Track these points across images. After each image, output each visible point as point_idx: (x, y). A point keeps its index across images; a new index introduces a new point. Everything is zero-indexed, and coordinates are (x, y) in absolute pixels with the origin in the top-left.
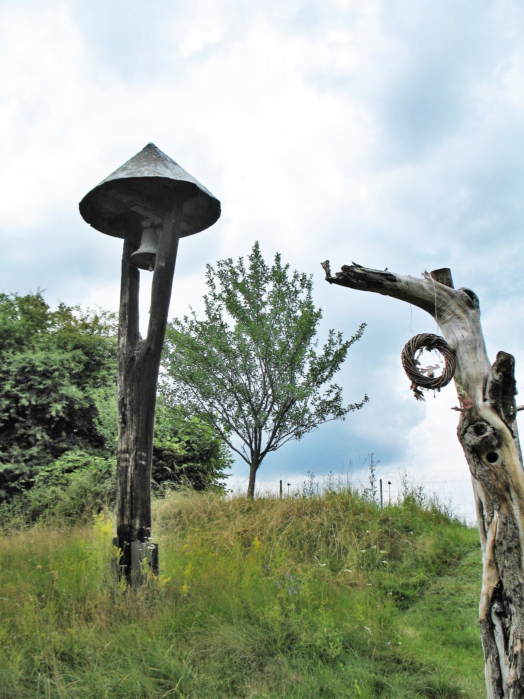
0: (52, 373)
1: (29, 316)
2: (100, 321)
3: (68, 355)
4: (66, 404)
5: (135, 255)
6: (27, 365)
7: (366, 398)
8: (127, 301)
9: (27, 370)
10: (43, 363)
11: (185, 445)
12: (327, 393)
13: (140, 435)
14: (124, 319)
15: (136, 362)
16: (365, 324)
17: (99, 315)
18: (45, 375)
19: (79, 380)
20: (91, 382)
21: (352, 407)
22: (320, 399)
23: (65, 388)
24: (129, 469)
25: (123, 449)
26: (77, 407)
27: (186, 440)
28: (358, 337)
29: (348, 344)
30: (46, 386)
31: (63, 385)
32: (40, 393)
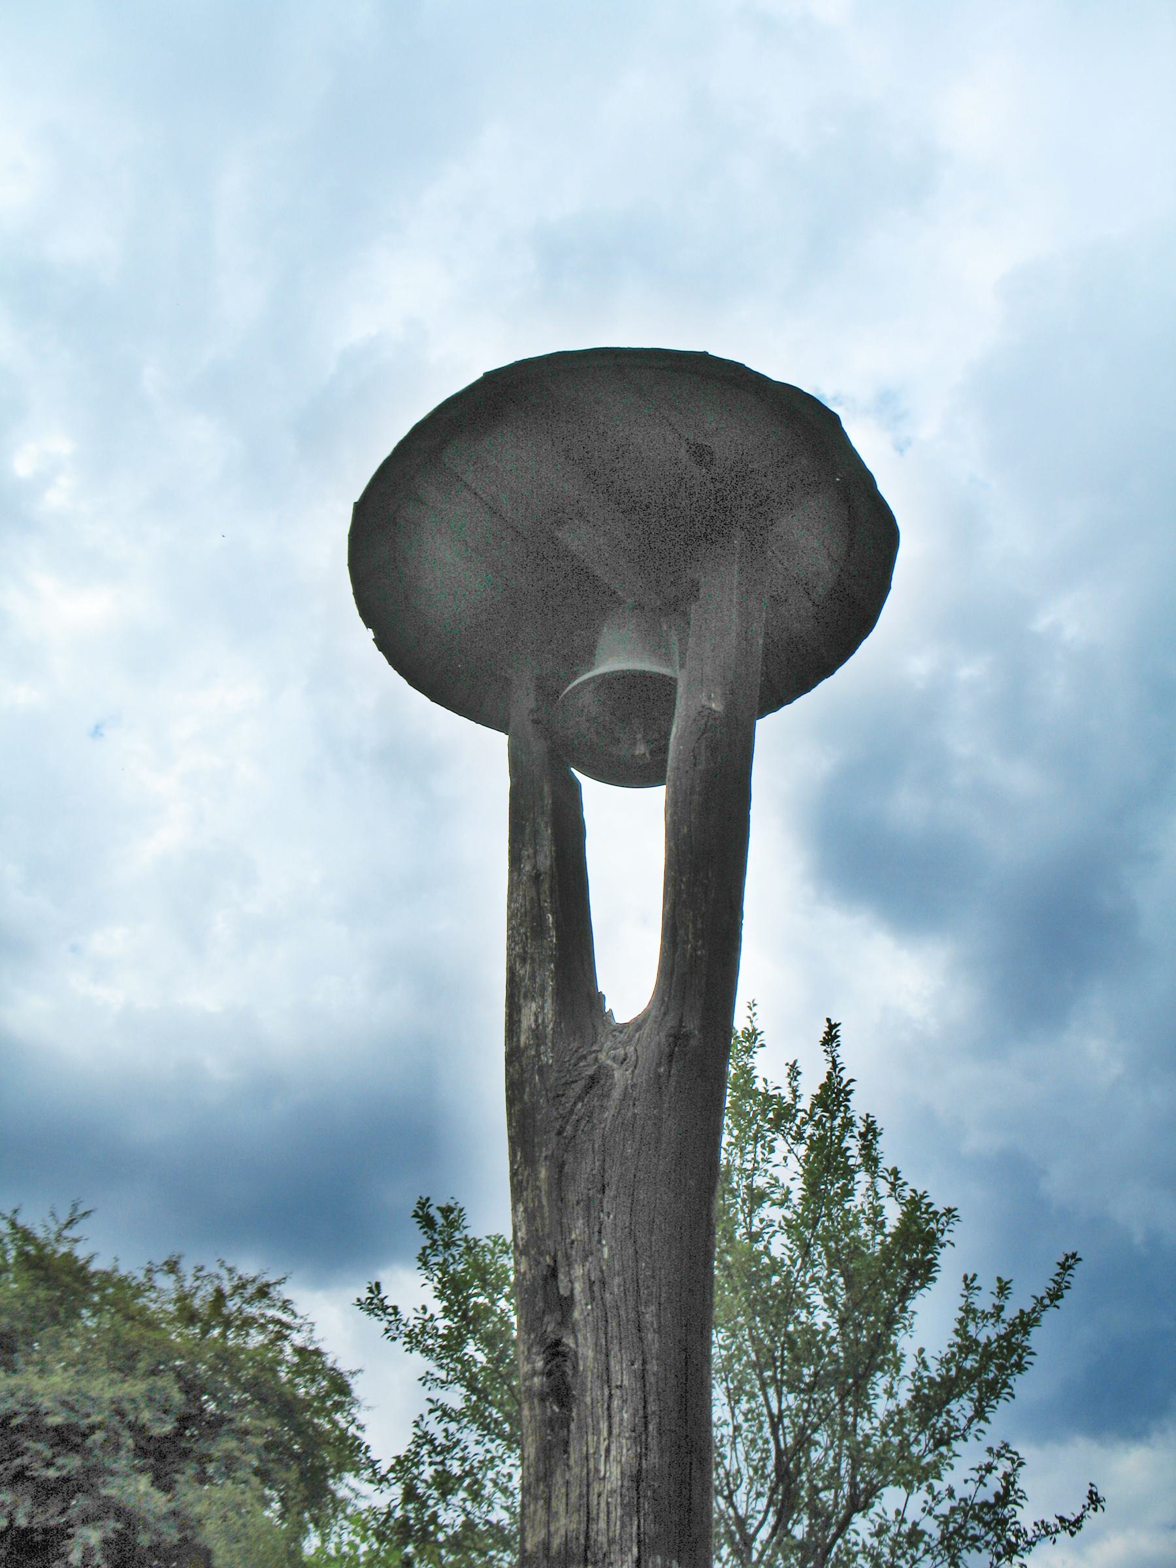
0: (85, 1436)
1: (41, 1273)
2: (230, 1304)
3: (136, 1387)
4: (115, 1531)
5: (580, 683)
6: (17, 1407)
7: (1094, 1500)
8: (545, 862)
9: (15, 1422)
10: (64, 1403)
12: (976, 1476)
13: (653, 1459)
14: (538, 931)
15: (616, 1094)
16: (1074, 1255)
17: (227, 1288)
18: (66, 1439)
19: (161, 1457)
20: (191, 1469)
21: (1046, 1531)
22: (951, 1493)
23: (119, 1481)
25: (556, 1542)
26: (144, 1539)
28: (1055, 1296)
29: (1025, 1322)
30: (64, 1472)
31: (112, 1473)
32: (46, 1491)
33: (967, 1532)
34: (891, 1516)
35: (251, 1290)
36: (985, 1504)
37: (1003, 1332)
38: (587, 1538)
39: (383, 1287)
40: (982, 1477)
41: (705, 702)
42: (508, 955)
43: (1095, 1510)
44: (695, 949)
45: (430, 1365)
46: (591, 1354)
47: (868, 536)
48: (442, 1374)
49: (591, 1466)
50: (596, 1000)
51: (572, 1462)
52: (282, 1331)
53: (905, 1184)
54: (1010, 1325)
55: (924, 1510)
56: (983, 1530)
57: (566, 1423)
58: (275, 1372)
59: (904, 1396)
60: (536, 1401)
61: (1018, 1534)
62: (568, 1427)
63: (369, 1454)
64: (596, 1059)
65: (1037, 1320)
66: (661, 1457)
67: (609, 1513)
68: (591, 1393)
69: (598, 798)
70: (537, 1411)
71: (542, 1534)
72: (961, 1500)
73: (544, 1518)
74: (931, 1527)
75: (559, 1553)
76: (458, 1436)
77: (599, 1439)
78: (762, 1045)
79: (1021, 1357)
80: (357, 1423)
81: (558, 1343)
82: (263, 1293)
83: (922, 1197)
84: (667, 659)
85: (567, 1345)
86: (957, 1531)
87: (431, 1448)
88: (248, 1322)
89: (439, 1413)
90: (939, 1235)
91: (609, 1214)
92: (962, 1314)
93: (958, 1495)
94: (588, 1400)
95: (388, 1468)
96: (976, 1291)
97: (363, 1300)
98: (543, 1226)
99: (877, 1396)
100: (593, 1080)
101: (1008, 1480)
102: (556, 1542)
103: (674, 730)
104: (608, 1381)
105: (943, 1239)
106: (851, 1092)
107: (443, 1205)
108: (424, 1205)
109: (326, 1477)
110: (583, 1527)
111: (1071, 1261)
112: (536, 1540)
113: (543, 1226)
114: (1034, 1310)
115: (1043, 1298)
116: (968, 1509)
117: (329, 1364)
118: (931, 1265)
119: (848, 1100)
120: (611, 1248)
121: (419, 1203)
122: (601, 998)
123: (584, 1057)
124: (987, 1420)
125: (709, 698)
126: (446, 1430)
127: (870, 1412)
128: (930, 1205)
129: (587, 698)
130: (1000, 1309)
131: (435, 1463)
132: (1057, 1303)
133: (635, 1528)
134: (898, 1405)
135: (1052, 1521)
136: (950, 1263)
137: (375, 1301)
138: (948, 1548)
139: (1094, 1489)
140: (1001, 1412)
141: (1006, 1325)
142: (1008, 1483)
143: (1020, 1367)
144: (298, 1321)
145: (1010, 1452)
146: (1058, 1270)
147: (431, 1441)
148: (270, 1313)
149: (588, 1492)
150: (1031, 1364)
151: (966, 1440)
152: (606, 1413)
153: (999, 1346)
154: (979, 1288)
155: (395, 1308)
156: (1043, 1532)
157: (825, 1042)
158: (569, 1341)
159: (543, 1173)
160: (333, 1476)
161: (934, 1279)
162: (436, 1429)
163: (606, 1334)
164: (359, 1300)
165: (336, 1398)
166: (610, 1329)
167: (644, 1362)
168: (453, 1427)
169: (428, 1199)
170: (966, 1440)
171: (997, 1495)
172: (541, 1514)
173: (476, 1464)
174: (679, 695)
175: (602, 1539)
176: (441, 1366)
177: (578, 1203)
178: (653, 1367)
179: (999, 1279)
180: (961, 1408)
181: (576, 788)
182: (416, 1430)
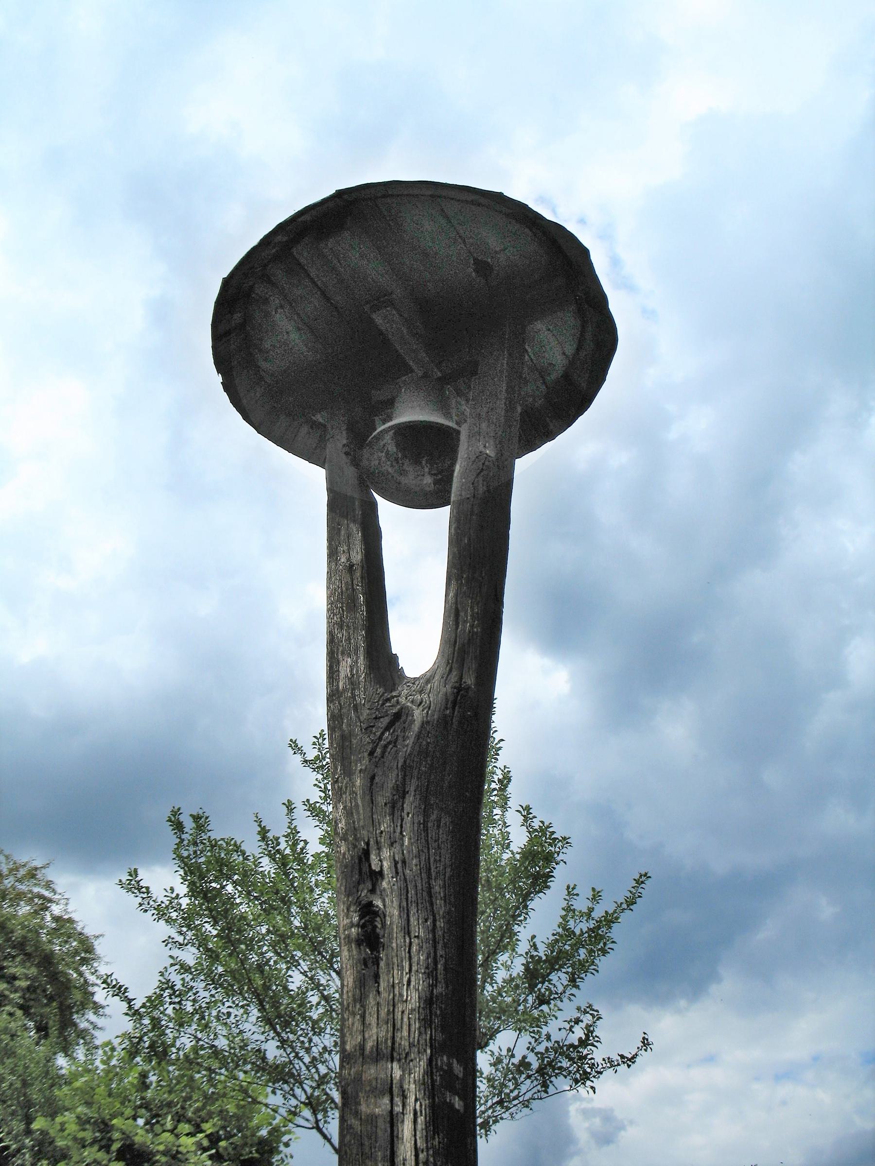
7: (646, 1043)
8: (357, 557)
11: (206, 1143)
12: (568, 1026)
14: (352, 605)
16: (646, 874)
21: (611, 1063)
22: (548, 1037)
24: (406, 1129)
25: (370, 1044)
27: (208, 1132)
28: (631, 902)
29: (609, 920)
33: (556, 1064)
34: (504, 1052)
35: (22, 872)
36: (572, 1045)
37: (592, 926)
38: (393, 1043)
39: (139, 872)
40: (572, 1027)
41: (481, 448)
42: (328, 622)
43: (646, 1050)
44: (472, 626)
45: (173, 932)
46: (396, 913)
47: (598, 340)
48: (180, 939)
49: (397, 992)
50: (393, 660)
51: (381, 989)
52: (45, 904)
53: (535, 817)
54: (597, 922)
55: (528, 1048)
56: (569, 1063)
57: (377, 961)
58: (38, 934)
59: (518, 968)
61: (592, 1066)
62: (378, 965)
63: (126, 994)
64: (398, 702)
65: (617, 918)
66: (447, 987)
67: (409, 1025)
68: (396, 940)
69: (389, 514)
70: (355, 952)
72: (556, 1042)
73: (360, 1028)
74: (532, 1059)
75: (371, 1052)
76: (191, 984)
77: (402, 973)
79: (605, 944)
80: (98, 973)
81: (370, 904)
82: (32, 874)
84: (447, 415)
85: (377, 906)
86: (550, 1064)
87: (171, 992)
88: (20, 896)
89: (177, 967)
90: (556, 855)
91: (408, 814)
92: (564, 913)
93: (553, 1039)
94: (394, 945)
95: (140, 1005)
96: (575, 897)
97: (124, 881)
98: (359, 820)
99: (498, 968)
100: (397, 716)
101: (589, 1031)
102: (370, 1044)
103: (457, 468)
104: (409, 933)
105: (558, 859)
106: (500, 748)
107: (195, 814)
108: (176, 813)
109: (71, 1014)
110: (390, 1034)
111: (643, 878)
112: (354, 1043)
113: (359, 820)
114: (615, 912)
115: (622, 903)
116: (561, 1049)
117: (79, 929)
118: (549, 876)
119: (498, 755)
120: (410, 839)
121: (172, 811)
122: (394, 659)
123: (388, 700)
124: (578, 987)
125: (485, 447)
126: (183, 979)
127: (492, 979)
128: (553, 833)
129: (388, 438)
130: (591, 910)
131: (174, 1003)
132: (631, 907)
133: (428, 1036)
134: (511, 975)
135: (615, 1057)
136: (561, 876)
137: (133, 882)
138: (542, 1075)
140: (588, 982)
141: (594, 922)
142: (589, 1031)
143: (604, 952)
144: (57, 897)
145: (593, 1010)
146: (634, 884)
147: (172, 987)
148: (36, 890)
149: (394, 1010)
152: (407, 955)
153: (590, 936)
154: (577, 895)
155: (147, 888)
156: (608, 1065)
158: (378, 903)
159: (358, 782)
160: (77, 1012)
161: (548, 887)
162: (176, 979)
163: (407, 899)
164: (120, 881)
165: (83, 955)
166: (410, 895)
167: (434, 921)
168: (188, 977)
169: (179, 809)
171: (580, 1039)
172: (358, 1026)
173: (204, 1005)
174: (461, 443)
175: (405, 1043)
176: (180, 933)
177: (386, 804)
178: (440, 924)
180: (559, 979)
181: (374, 506)
182: (161, 978)
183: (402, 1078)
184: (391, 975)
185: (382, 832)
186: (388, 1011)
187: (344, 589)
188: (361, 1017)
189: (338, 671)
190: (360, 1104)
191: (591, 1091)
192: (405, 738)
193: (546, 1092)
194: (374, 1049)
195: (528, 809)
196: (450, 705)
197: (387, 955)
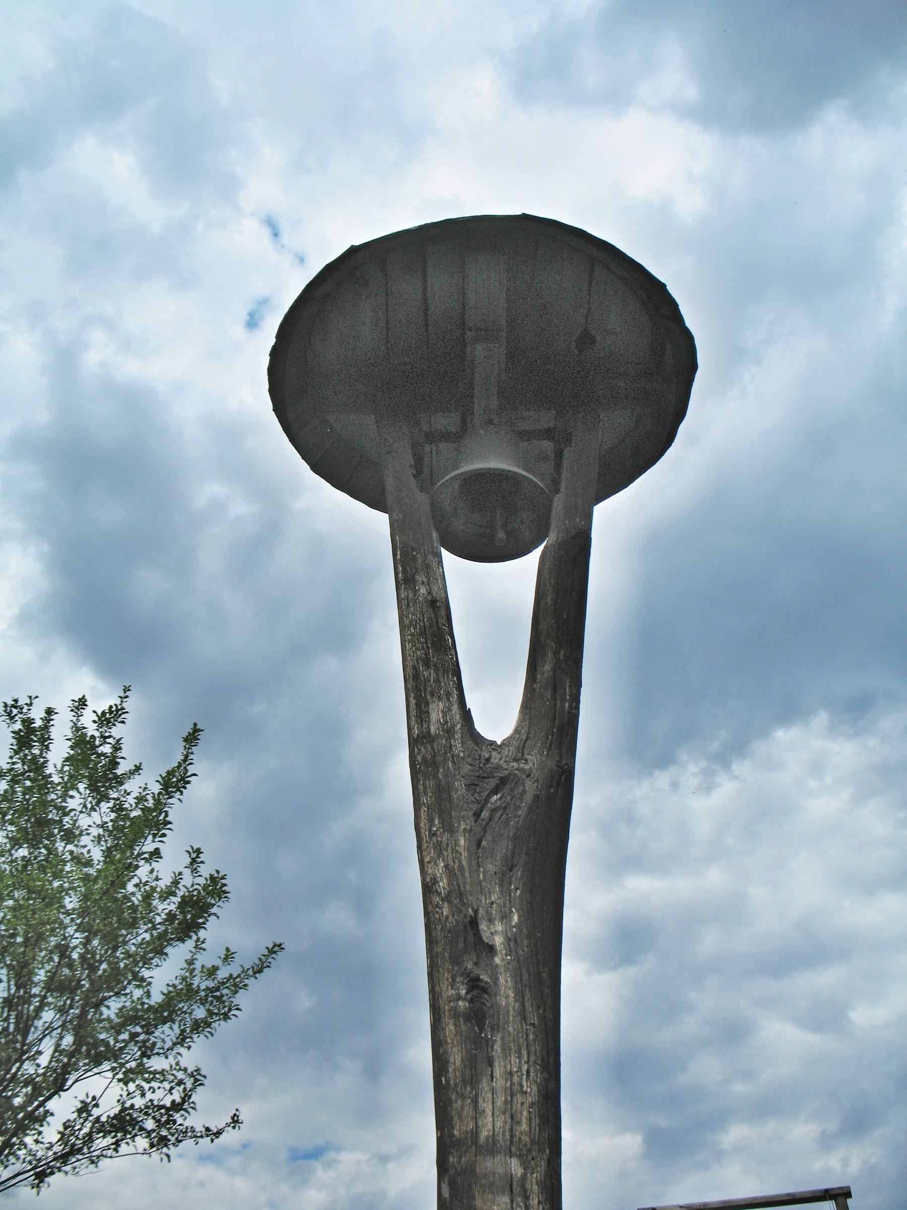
16: (280, 945)
29: (236, 984)
38: (512, 1136)
43: (234, 1128)
55: (119, 1101)
60: (462, 1021)
71: (471, 1125)
78: (123, 722)
83: (223, 878)
101: (186, 1097)
106: (189, 782)
110: (508, 1127)
114: (239, 976)
119: (185, 788)
128: (224, 885)
132: (257, 975)
139: (238, 1113)
143: (226, 1017)
149: (511, 1101)
150: (236, 1016)
151: (167, 1057)
157: (186, 740)
159: (462, 842)
170: (167, 1057)
177: (495, 873)
179: (228, 949)
183: (524, 1177)
184: (508, 1062)
185: (492, 903)
186: (506, 1099)
187: (427, 624)
188: (472, 1101)
189: (428, 712)
190: (474, 1199)
191: (165, 1158)
192: (518, 808)
193: (116, 1150)
194: (490, 1140)
195: (198, 851)
196: (555, 783)
197: (502, 1038)
